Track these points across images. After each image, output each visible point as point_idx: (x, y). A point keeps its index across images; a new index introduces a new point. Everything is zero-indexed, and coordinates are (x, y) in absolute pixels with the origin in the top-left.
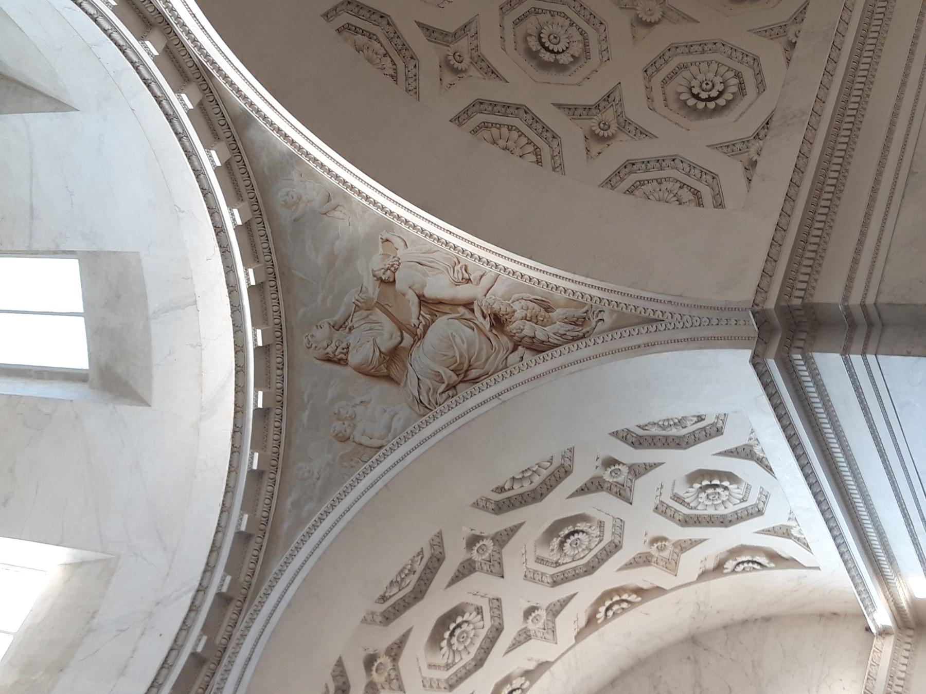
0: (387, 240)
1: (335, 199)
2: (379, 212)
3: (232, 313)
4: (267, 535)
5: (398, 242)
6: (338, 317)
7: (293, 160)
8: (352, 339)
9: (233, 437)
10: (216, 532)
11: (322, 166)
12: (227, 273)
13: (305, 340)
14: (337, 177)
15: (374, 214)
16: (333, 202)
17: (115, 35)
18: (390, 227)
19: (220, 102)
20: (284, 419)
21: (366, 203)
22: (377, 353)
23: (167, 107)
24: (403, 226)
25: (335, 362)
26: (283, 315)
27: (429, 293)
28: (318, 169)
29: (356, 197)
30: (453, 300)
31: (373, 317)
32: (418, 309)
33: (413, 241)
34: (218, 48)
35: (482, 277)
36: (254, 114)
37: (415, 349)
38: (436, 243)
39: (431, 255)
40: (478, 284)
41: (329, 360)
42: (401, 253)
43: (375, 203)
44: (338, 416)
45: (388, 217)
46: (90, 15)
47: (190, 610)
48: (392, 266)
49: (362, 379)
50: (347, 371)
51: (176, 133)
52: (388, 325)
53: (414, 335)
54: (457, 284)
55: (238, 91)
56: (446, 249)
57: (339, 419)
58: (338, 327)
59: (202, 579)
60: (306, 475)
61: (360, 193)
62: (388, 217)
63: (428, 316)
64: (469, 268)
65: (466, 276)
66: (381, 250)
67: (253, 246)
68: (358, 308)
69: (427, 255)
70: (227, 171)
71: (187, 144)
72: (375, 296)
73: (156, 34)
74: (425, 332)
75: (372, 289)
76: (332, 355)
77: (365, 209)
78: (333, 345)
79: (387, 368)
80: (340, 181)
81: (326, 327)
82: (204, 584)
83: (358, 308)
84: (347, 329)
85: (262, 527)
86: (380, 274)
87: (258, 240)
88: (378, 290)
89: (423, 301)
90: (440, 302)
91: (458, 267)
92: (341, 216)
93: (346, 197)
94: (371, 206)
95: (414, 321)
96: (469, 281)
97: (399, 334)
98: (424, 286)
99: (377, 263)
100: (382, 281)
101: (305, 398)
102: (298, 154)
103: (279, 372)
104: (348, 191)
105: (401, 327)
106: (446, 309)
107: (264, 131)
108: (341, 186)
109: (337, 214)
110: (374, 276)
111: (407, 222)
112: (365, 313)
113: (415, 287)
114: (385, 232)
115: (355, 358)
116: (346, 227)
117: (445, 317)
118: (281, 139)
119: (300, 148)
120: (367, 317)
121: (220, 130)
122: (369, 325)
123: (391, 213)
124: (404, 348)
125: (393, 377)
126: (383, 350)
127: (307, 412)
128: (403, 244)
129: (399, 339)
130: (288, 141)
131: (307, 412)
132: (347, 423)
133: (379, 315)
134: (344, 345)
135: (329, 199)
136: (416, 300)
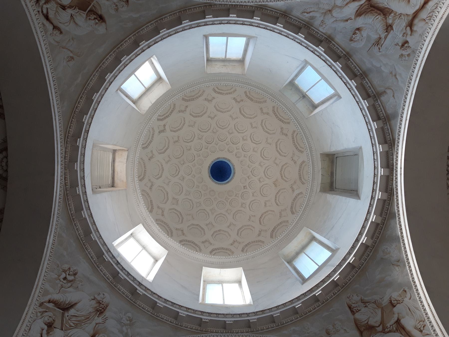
0: (405, 291)
1: (401, 263)
2: (411, 279)
3: (338, 265)
4: (278, 327)
5: (408, 296)
6: (366, 299)
7: (398, 240)
8: (363, 310)
9: (301, 295)
10: (268, 309)
11: (405, 248)
12: (347, 254)
13: (349, 295)
14: (407, 255)
15: (409, 279)
16: (399, 264)
17: (376, 162)
18: (410, 288)
19: (390, 205)
20: (319, 307)
21: (409, 272)
22: (366, 322)
23: (374, 194)
24: (415, 290)
25: (351, 310)
26: (351, 281)
27: (403, 321)
28: (404, 252)
29: (407, 267)
30: (409, 332)
31: (376, 310)
32: (393, 323)
33: (414, 300)
34: (401, 182)
35: (428, 334)
36: (397, 215)
37: (380, 334)
38: (421, 306)
39: (416, 310)
40: (423, 336)
41: (350, 308)
42: (406, 300)
43: (412, 275)
44: (334, 325)
45: (412, 283)
46: (373, 151)
47: (239, 314)
48: (399, 301)
49: (353, 324)
50: (352, 317)
51: (370, 204)
52: (378, 318)
53: (384, 329)
54: (416, 328)
55: (398, 204)
56: (423, 311)
57: (333, 326)
58: (363, 301)
59: (251, 313)
60: (307, 328)
61: (410, 267)
62: (412, 283)
63: (394, 328)
64: (426, 327)
65: (422, 329)
66: (400, 292)
67: (363, 255)
68: (375, 302)
69: (414, 309)
70: (375, 225)
71: (371, 209)
72: (384, 305)
73: (387, 170)
74: (388, 332)
75: (385, 302)
76: (352, 307)
77: (407, 275)
78: (356, 305)
79: (364, 330)
80: (406, 258)
81: (359, 298)
82: (250, 315)
83: (375, 302)
84: (365, 305)
85: (280, 324)
86: (393, 299)
87: (366, 254)
88: (387, 303)
89: (398, 322)
90: (403, 328)
91: (421, 323)
92: (398, 270)
93: (405, 265)
94: (410, 274)
95: (388, 325)
96: (421, 331)
97: (379, 324)
98: (403, 318)
99: (395, 295)
100: (391, 302)
101: (331, 309)
102: (401, 238)
103: (333, 294)
104: (407, 264)
105: (382, 322)
106: (404, 333)
107: (396, 224)
108: (405, 259)
109: (397, 268)
110: (390, 298)
111: (417, 290)
112: (375, 306)
113: (400, 315)
114: (407, 287)
115: (357, 316)
116: (396, 274)
117: (401, 335)
118: (399, 229)
119: (403, 237)
120: (375, 308)
121: (384, 213)
122: (373, 311)
123: (415, 282)
124: (376, 330)
125: (363, 334)
126: (369, 323)
127: (327, 313)
128: (409, 297)
129: (377, 325)
130: (401, 231)
131: (327, 313)
132: (334, 330)
133: (379, 312)
134: (359, 309)
135: (398, 261)
136: (396, 319)
